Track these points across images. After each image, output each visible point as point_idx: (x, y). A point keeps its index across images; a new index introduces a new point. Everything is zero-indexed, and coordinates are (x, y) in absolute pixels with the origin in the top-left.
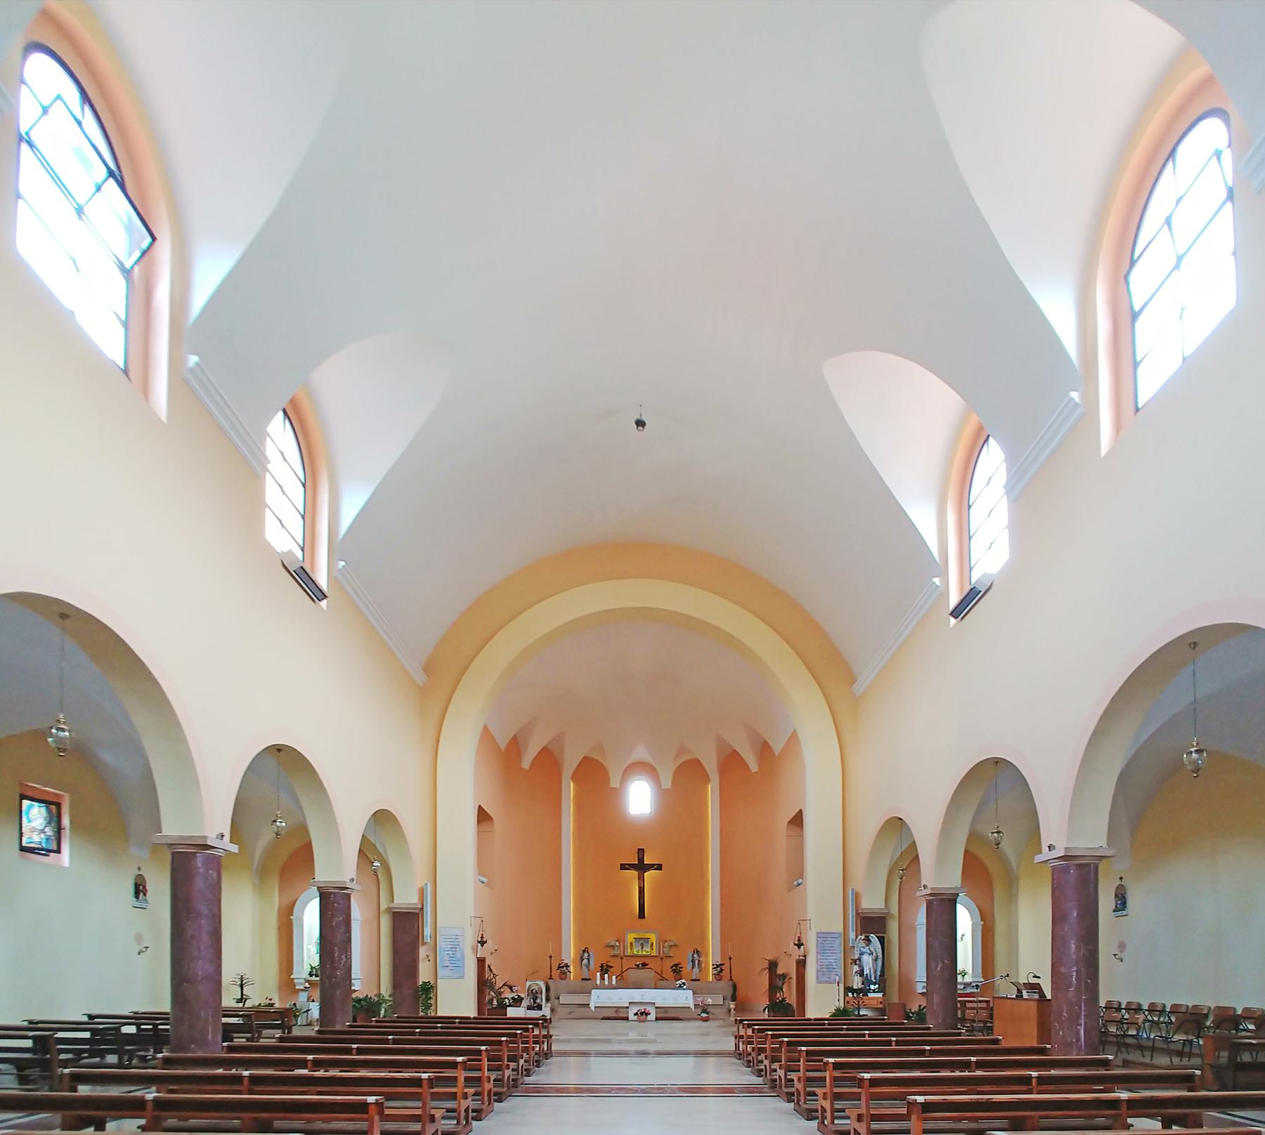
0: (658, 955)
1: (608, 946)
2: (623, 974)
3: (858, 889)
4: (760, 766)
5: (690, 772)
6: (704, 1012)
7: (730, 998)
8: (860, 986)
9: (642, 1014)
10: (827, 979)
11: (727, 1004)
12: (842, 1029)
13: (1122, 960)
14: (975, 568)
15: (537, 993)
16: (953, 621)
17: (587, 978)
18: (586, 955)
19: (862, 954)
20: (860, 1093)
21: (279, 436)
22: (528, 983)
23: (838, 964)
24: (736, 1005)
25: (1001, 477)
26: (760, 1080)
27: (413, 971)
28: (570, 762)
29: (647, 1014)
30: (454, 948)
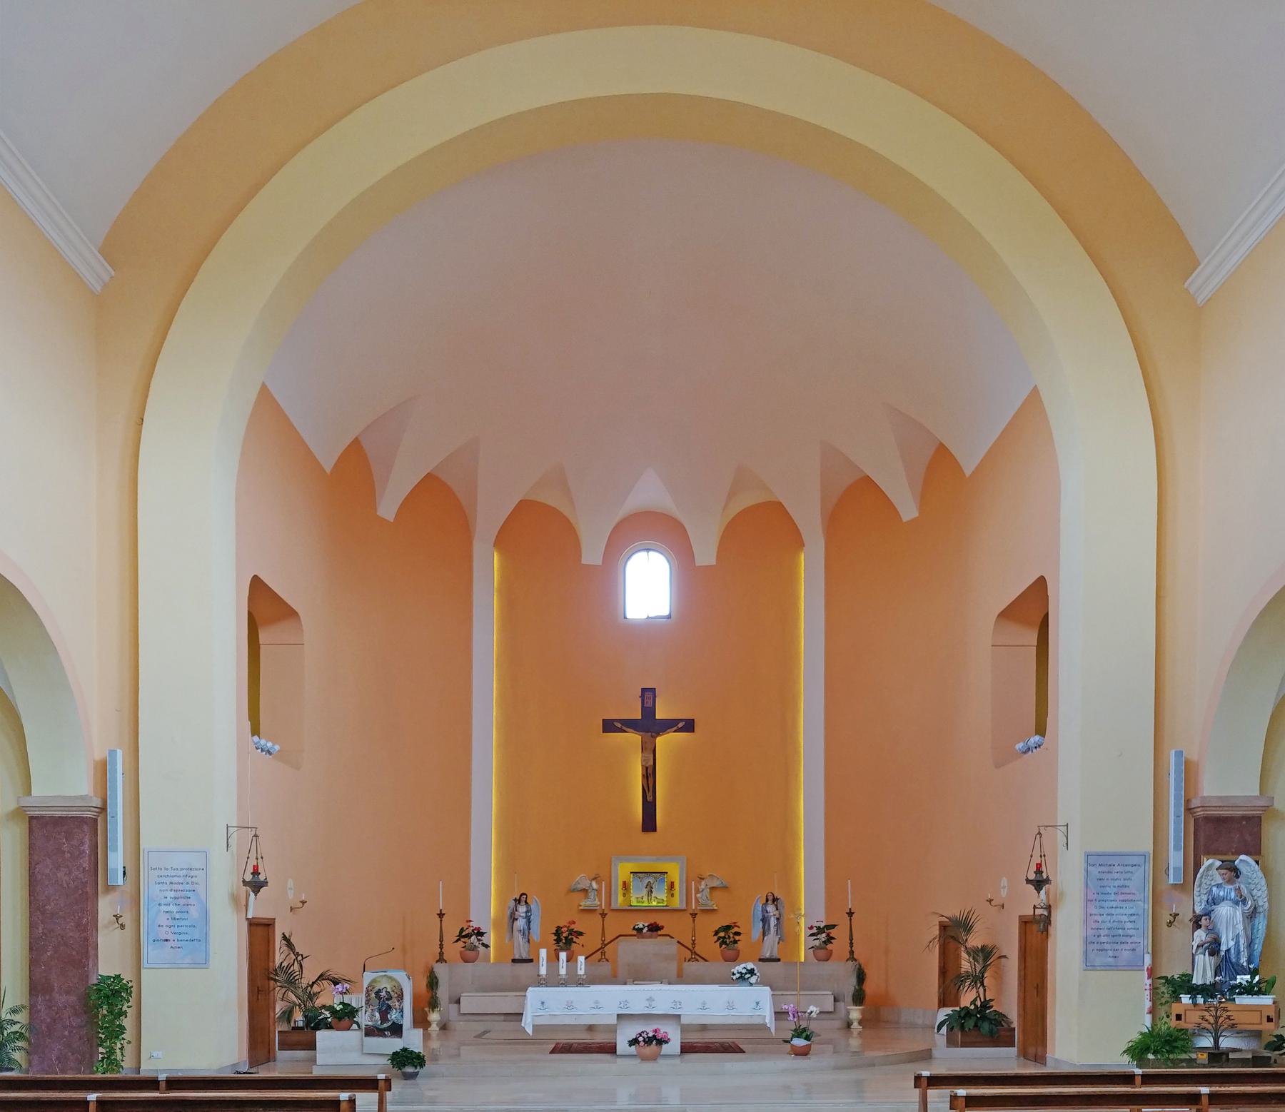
0: (684, 907)
2: (606, 949)
6: (799, 1033)
7: (849, 999)
8: (1210, 979)
9: (648, 1041)
10: (1111, 960)
11: (842, 1014)
15: (390, 998)
17: (525, 956)
19: (1214, 901)
22: (368, 977)
23: (1140, 925)
24: (863, 1013)
27: (85, 950)
29: (661, 1041)
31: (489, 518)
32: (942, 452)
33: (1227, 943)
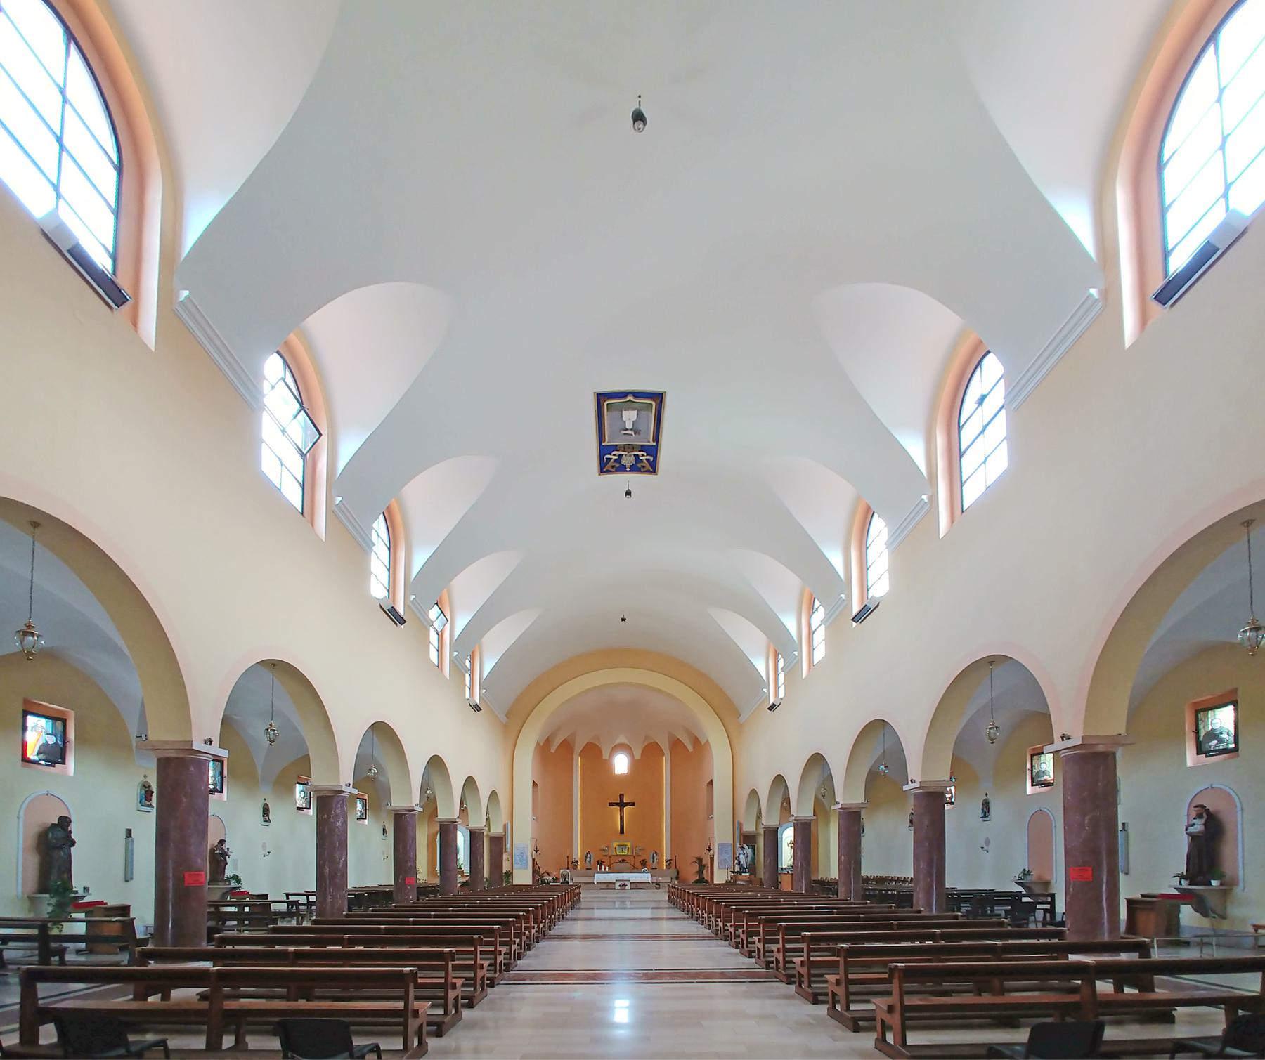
1: (601, 850)
3: (742, 821)
4: (694, 748)
5: (652, 750)
12: (812, 908)
13: (987, 852)
14: (966, 484)
16: (854, 624)
18: (589, 855)
19: (739, 854)
20: (838, 961)
21: (380, 525)
22: (561, 871)
25: (885, 536)
28: (579, 746)
30: (522, 854)
31: (578, 748)
32: (696, 738)
33: (742, 863)
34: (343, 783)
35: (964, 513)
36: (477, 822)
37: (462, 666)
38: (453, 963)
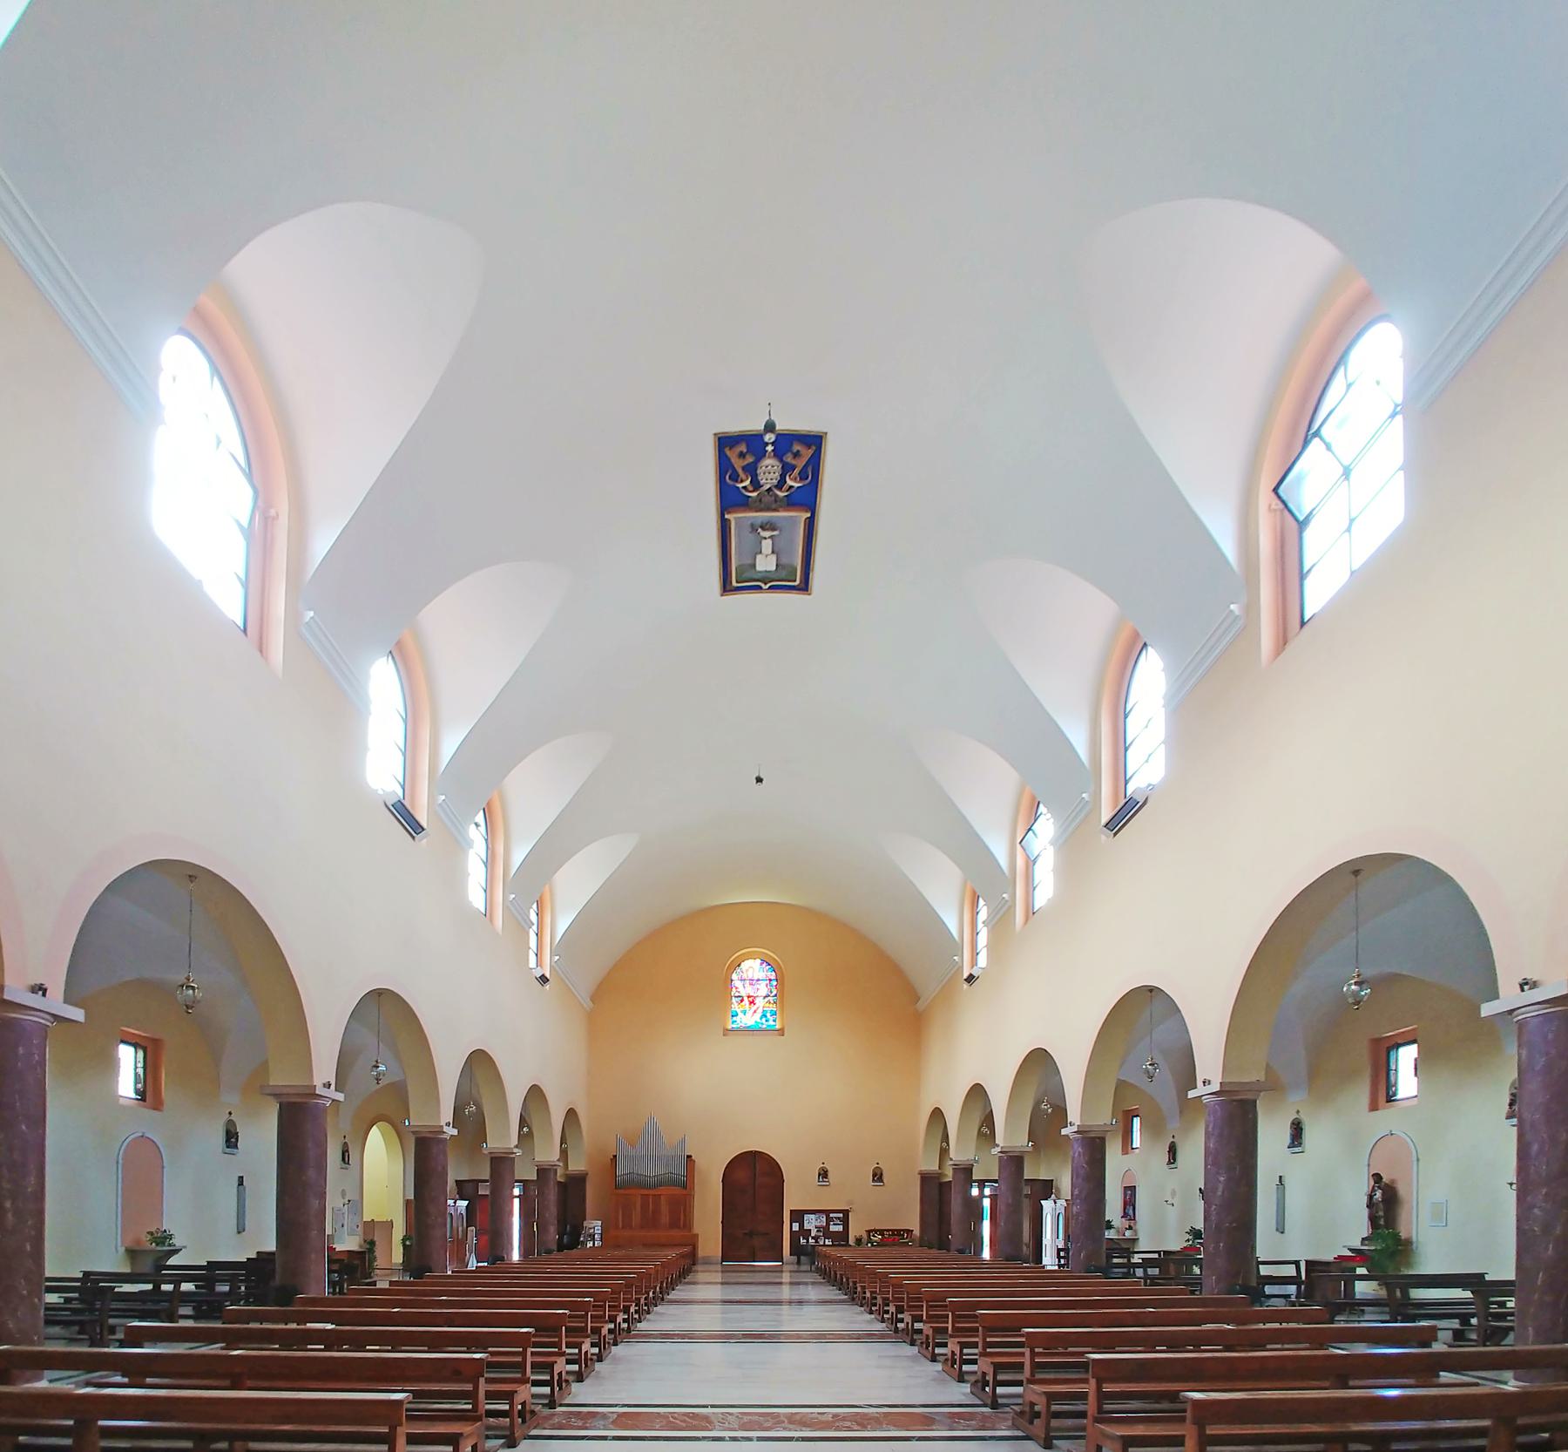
25: (1394, 387)
26: (846, 1297)
34: (443, 1123)
35: (1306, 628)
36: (548, 1153)
37: (525, 921)
38: (533, 1350)
